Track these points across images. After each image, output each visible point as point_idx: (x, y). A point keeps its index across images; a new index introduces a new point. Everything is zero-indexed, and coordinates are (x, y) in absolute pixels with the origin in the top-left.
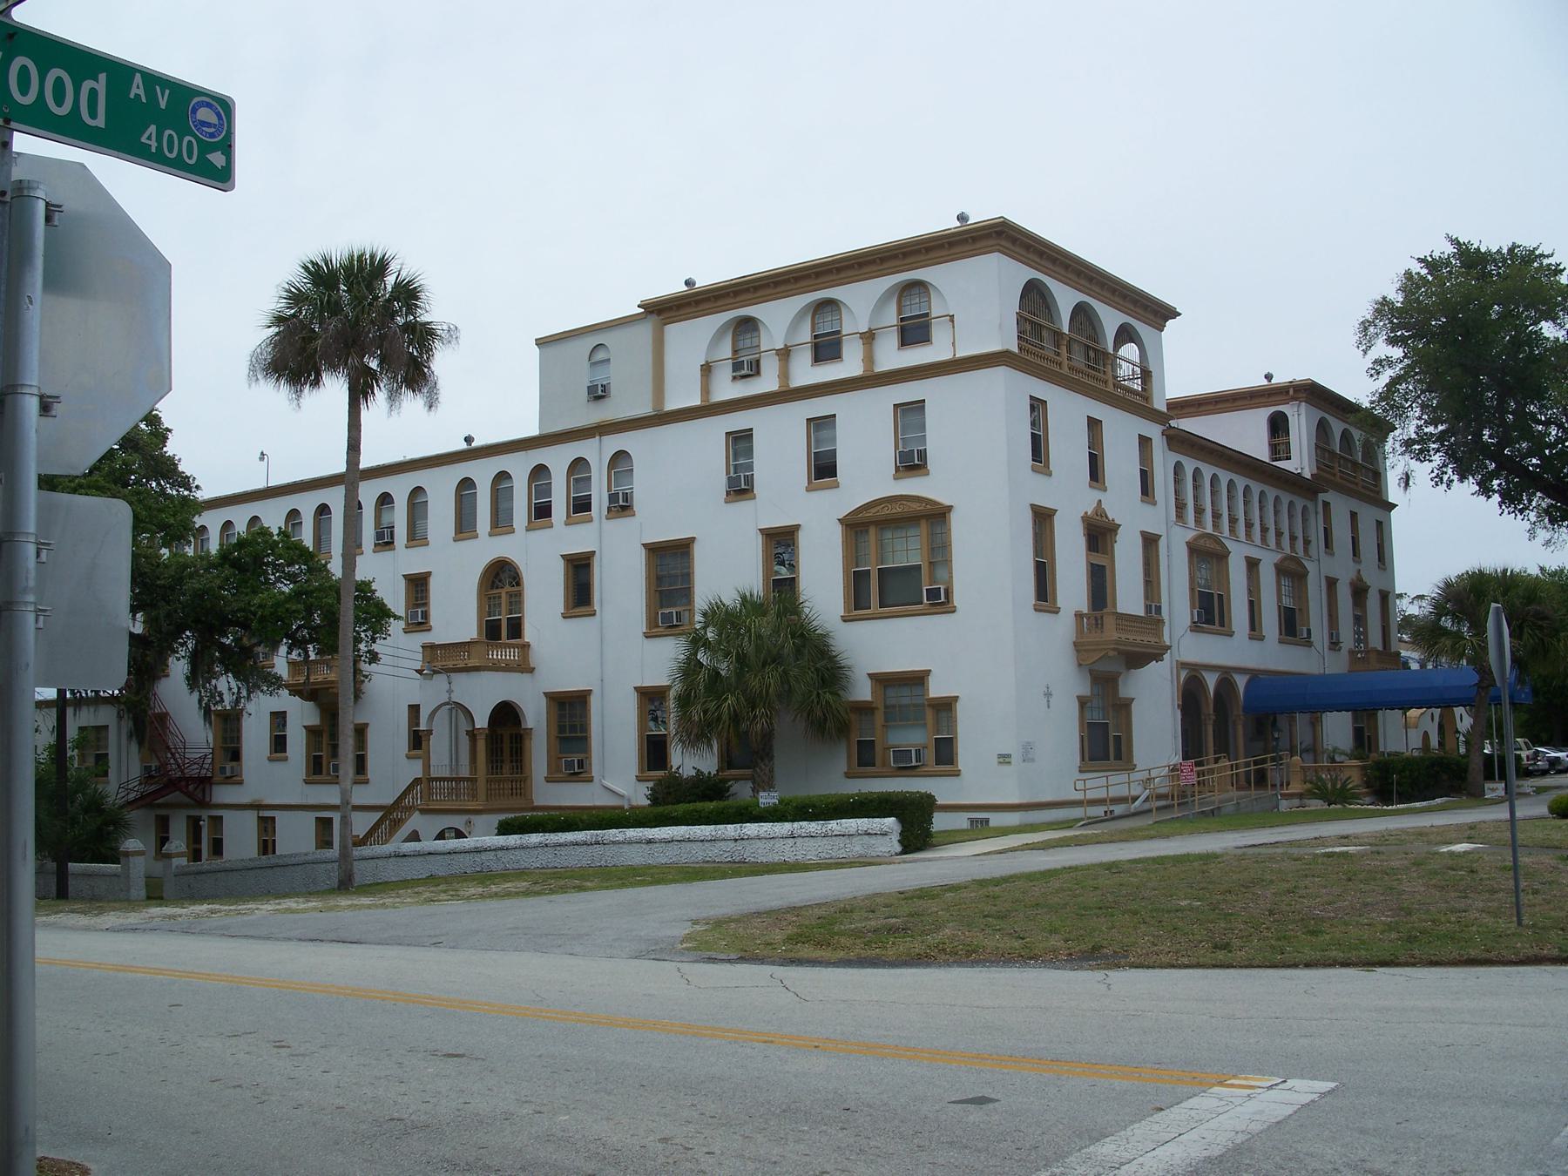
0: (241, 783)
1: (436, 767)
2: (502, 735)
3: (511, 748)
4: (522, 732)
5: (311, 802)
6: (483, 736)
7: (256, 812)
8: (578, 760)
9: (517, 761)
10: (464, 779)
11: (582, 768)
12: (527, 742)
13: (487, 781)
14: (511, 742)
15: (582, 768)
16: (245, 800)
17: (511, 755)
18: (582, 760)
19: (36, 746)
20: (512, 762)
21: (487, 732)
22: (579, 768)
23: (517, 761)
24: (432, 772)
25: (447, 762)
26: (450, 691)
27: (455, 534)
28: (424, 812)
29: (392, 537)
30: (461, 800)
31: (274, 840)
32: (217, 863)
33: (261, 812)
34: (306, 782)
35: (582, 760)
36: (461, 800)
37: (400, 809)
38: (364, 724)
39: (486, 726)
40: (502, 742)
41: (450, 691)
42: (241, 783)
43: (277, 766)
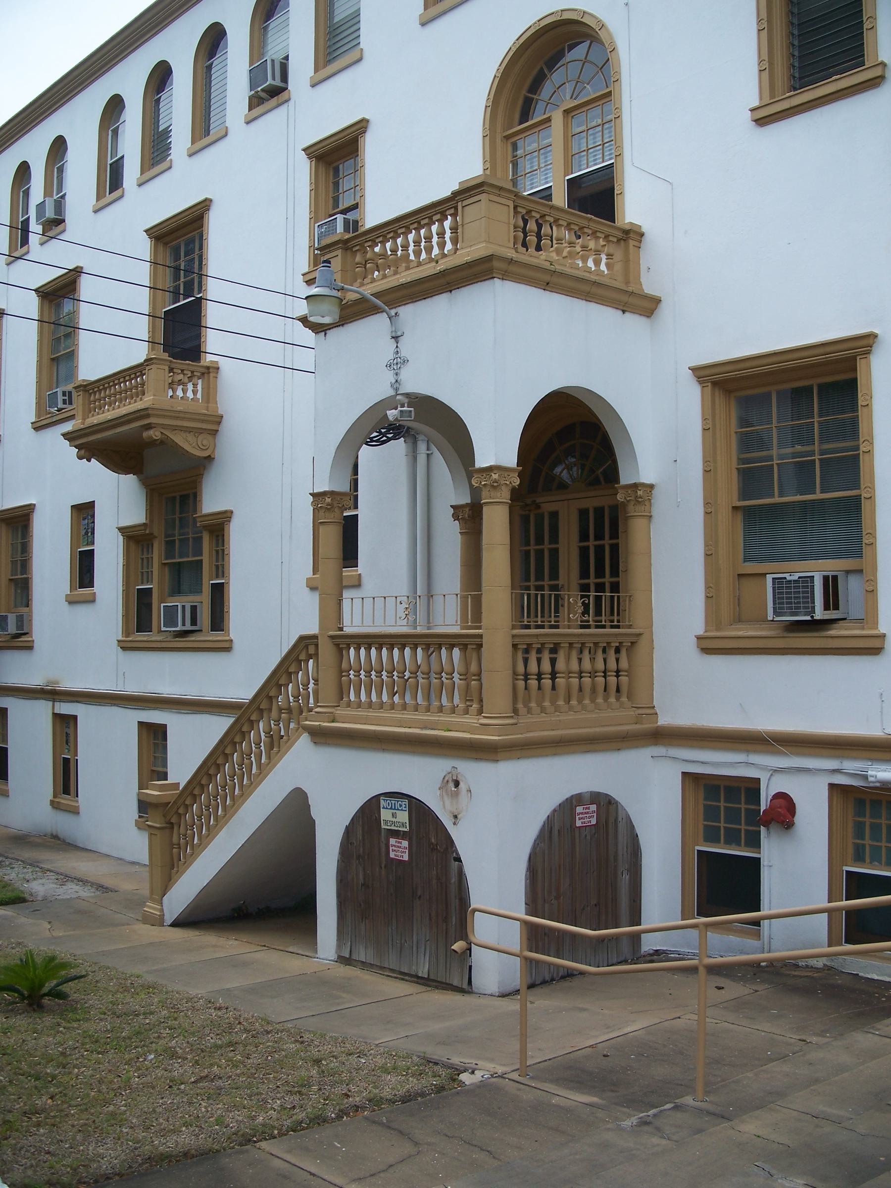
0: (30, 647)
1: (379, 602)
2: (554, 515)
3: (584, 553)
4: (620, 497)
5: (132, 688)
6: (505, 495)
7: (51, 703)
8: (826, 579)
9: (600, 588)
10: (450, 641)
11: (836, 607)
12: (637, 525)
13: (515, 646)
14: (584, 536)
15: (836, 607)
16: (35, 681)
17: (584, 573)
18: (835, 578)
19: (741, 704)
20: (585, 588)
21: (517, 482)
22: (827, 607)
23: (600, 588)
24: (346, 620)
25: (402, 588)
26: (397, 364)
27: (426, 8)
28: (321, 736)
29: (284, 77)
30: (441, 709)
31: (77, 760)
32: (826, 573)
33: (57, 704)
34: (125, 647)
35: (835, 578)
36: (441, 709)
37: (274, 713)
38: (226, 512)
39: (510, 459)
40: (554, 538)
41: (397, 364)
42: (30, 647)
43: (82, 610)
